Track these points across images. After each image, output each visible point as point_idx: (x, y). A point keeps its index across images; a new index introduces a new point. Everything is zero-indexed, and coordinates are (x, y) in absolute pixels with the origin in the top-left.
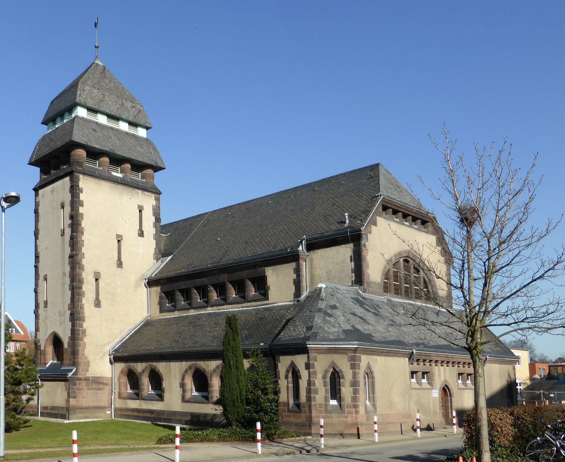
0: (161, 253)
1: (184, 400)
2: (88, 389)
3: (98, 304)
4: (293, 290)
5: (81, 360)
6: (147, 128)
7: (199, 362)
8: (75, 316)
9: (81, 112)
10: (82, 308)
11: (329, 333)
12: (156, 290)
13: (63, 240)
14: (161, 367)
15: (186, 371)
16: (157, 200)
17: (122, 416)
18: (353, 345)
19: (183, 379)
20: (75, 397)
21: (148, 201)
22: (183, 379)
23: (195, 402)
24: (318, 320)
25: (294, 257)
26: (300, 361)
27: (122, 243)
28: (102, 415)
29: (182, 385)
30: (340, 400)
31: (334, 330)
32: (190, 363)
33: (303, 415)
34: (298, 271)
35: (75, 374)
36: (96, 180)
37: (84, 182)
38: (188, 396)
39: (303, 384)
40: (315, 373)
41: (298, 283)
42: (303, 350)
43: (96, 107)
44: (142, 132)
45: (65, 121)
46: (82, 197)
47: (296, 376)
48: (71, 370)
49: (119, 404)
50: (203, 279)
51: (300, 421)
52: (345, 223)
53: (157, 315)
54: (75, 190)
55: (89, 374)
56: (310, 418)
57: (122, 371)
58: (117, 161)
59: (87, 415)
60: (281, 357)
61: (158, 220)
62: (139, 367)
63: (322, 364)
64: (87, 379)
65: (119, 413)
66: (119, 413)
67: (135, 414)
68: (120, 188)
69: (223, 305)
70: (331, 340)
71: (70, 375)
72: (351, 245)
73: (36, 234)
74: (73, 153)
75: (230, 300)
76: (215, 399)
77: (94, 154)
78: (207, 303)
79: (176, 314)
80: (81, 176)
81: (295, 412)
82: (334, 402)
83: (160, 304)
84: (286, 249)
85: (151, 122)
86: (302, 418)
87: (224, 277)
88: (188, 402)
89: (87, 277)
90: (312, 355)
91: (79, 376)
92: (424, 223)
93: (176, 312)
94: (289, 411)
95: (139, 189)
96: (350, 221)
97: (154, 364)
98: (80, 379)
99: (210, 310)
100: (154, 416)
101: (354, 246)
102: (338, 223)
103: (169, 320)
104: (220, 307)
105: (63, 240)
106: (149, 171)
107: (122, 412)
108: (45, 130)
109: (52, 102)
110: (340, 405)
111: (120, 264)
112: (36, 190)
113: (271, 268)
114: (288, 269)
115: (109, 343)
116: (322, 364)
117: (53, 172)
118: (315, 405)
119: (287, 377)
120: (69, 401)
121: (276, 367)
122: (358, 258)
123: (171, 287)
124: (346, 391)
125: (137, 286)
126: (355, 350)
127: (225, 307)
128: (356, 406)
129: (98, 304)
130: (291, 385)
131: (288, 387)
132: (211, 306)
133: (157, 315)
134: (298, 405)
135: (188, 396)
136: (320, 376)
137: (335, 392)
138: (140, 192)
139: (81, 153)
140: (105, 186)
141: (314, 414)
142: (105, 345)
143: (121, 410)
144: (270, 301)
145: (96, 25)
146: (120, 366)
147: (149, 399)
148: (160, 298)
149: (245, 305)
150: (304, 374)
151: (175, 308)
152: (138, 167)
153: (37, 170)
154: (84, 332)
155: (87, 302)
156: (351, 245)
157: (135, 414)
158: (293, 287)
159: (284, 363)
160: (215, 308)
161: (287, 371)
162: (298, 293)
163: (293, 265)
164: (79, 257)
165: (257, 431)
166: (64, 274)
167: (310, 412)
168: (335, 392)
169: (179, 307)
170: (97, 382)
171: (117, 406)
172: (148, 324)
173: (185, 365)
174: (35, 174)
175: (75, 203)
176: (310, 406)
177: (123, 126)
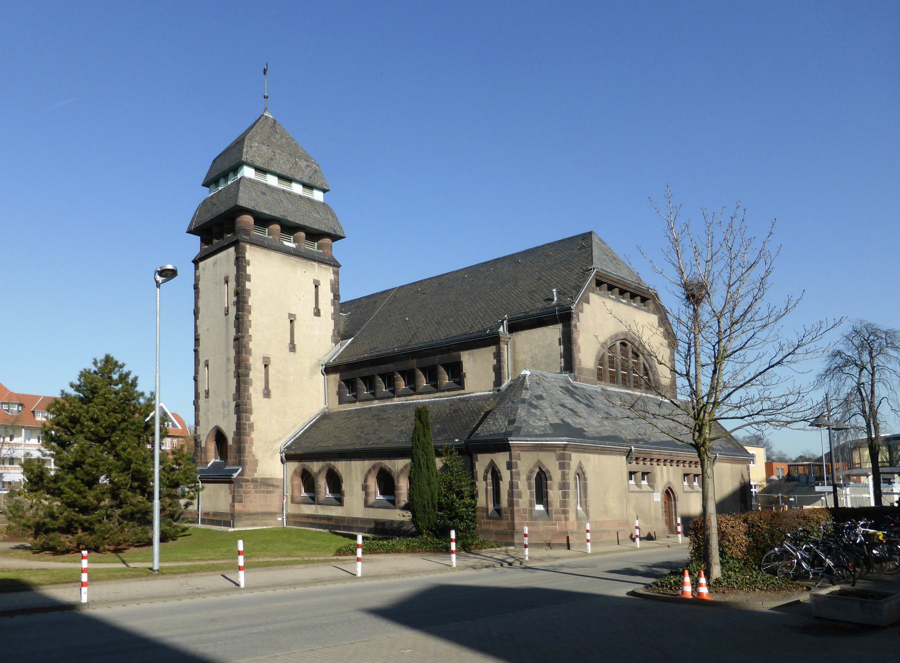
0: (340, 335)
1: (367, 505)
2: (256, 492)
3: (267, 394)
4: (492, 375)
5: (247, 458)
6: (325, 191)
7: (384, 461)
8: (241, 408)
9: (248, 172)
10: (249, 398)
11: (534, 428)
12: (335, 377)
13: (227, 320)
14: (340, 466)
15: (369, 472)
16: (336, 273)
17: (295, 523)
18: (562, 441)
19: (366, 480)
20: (241, 502)
21: (326, 275)
22: (366, 480)
23: (380, 507)
24: (522, 412)
25: (493, 340)
26: (501, 459)
27: (296, 323)
28: (272, 522)
29: (365, 488)
30: (547, 505)
31: (540, 423)
32: (373, 462)
33: (504, 522)
34: (498, 356)
35: (241, 474)
36: (266, 251)
37: (252, 254)
38: (371, 500)
39: (504, 486)
40: (518, 474)
41: (498, 370)
42: (502, 446)
43: (265, 167)
44: (318, 196)
45: (229, 183)
46: (249, 270)
47: (496, 477)
48: (236, 470)
49: (292, 509)
50: (389, 366)
51: (501, 528)
52: (553, 300)
53: (335, 406)
54: (240, 263)
55: (258, 475)
56: (512, 526)
57: (295, 472)
58: (289, 229)
59: (255, 522)
60: (479, 455)
61: (336, 296)
62: (315, 467)
63: (526, 463)
64: (254, 481)
65: (291, 519)
66: (291, 519)
67: (311, 521)
68: (293, 259)
69: (412, 395)
70: (537, 436)
71: (235, 475)
72: (560, 326)
73: (196, 313)
74: (238, 219)
75: (420, 389)
76: (403, 504)
77: (263, 221)
78: (394, 393)
79: (358, 406)
80: (248, 246)
81: (496, 519)
82: (540, 507)
83: (340, 394)
84: (485, 331)
85: (329, 184)
86: (503, 526)
87: (413, 363)
88: (371, 507)
89: (255, 362)
90: (515, 453)
91: (245, 477)
92: (644, 300)
93: (358, 403)
94: (488, 517)
95: (315, 261)
96: (558, 298)
97: (332, 463)
98: (247, 481)
99: (396, 401)
100: (333, 523)
101: (563, 327)
102: (545, 300)
103: (349, 412)
104: (409, 398)
105: (227, 320)
106: (327, 241)
107: (294, 519)
108: (207, 193)
109: (215, 161)
110: (547, 511)
111: (293, 348)
112: (196, 262)
113: (467, 352)
114: (488, 353)
115: (280, 439)
116: (526, 463)
117: (215, 241)
118: (519, 511)
119: (485, 478)
120: (234, 506)
121: (472, 467)
122: (568, 341)
123: (353, 374)
124: (554, 494)
125: (313, 373)
126: (565, 447)
127: (414, 397)
128: (565, 512)
129: (267, 394)
130: (490, 488)
131: (487, 489)
132: (398, 396)
133: (335, 407)
134: (498, 511)
135: (371, 500)
136: (523, 477)
137: (541, 496)
138: (316, 264)
139: (248, 219)
140: (276, 258)
141: (517, 521)
142: (276, 441)
143: (294, 516)
144: (467, 390)
145: (265, 71)
146: (293, 466)
147: (327, 503)
148: (340, 387)
149: (437, 395)
150: (505, 474)
151: (356, 399)
152: (314, 235)
153: (197, 239)
154: (251, 426)
155: (255, 391)
156: (560, 326)
157: (311, 521)
158: (493, 374)
159: (482, 462)
160: (402, 398)
161: (486, 472)
162: (498, 381)
163: (493, 349)
164: (246, 340)
165: (452, 540)
166: (228, 359)
167: (513, 518)
168: (541, 496)
169: (361, 397)
170: (267, 484)
171: (290, 511)
172: (325, 417)
173: (367, 464)
174: (195, 244)
175: (241, 276)
176: (512, 512)
177: (297, 189)
